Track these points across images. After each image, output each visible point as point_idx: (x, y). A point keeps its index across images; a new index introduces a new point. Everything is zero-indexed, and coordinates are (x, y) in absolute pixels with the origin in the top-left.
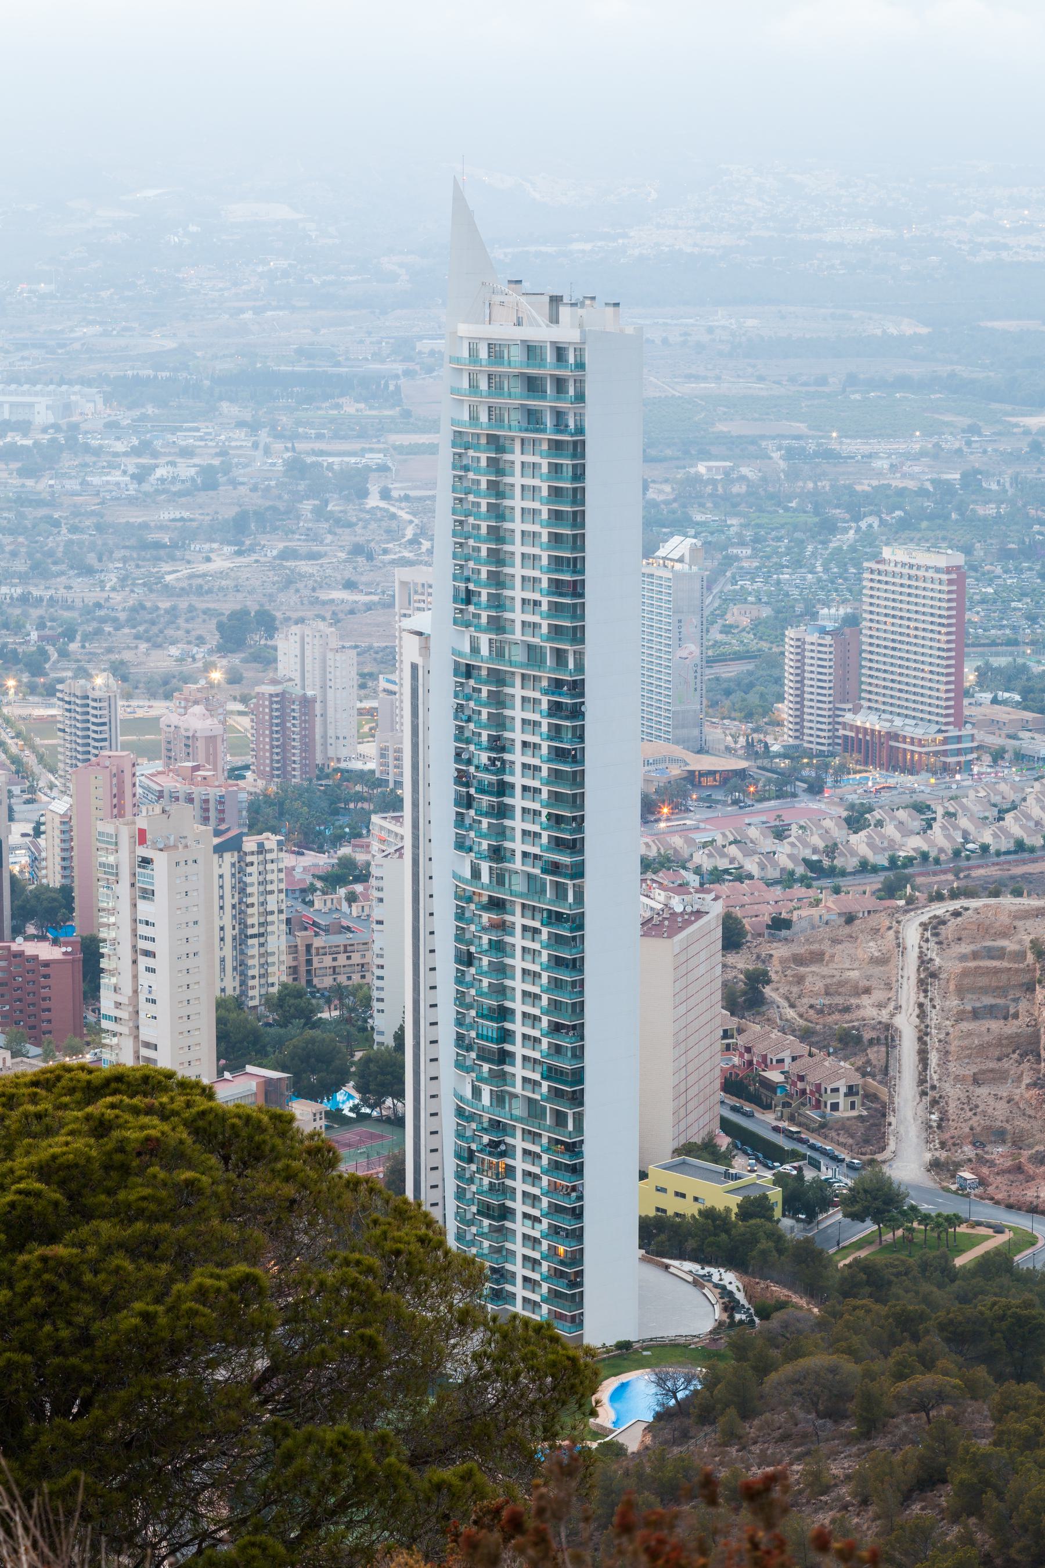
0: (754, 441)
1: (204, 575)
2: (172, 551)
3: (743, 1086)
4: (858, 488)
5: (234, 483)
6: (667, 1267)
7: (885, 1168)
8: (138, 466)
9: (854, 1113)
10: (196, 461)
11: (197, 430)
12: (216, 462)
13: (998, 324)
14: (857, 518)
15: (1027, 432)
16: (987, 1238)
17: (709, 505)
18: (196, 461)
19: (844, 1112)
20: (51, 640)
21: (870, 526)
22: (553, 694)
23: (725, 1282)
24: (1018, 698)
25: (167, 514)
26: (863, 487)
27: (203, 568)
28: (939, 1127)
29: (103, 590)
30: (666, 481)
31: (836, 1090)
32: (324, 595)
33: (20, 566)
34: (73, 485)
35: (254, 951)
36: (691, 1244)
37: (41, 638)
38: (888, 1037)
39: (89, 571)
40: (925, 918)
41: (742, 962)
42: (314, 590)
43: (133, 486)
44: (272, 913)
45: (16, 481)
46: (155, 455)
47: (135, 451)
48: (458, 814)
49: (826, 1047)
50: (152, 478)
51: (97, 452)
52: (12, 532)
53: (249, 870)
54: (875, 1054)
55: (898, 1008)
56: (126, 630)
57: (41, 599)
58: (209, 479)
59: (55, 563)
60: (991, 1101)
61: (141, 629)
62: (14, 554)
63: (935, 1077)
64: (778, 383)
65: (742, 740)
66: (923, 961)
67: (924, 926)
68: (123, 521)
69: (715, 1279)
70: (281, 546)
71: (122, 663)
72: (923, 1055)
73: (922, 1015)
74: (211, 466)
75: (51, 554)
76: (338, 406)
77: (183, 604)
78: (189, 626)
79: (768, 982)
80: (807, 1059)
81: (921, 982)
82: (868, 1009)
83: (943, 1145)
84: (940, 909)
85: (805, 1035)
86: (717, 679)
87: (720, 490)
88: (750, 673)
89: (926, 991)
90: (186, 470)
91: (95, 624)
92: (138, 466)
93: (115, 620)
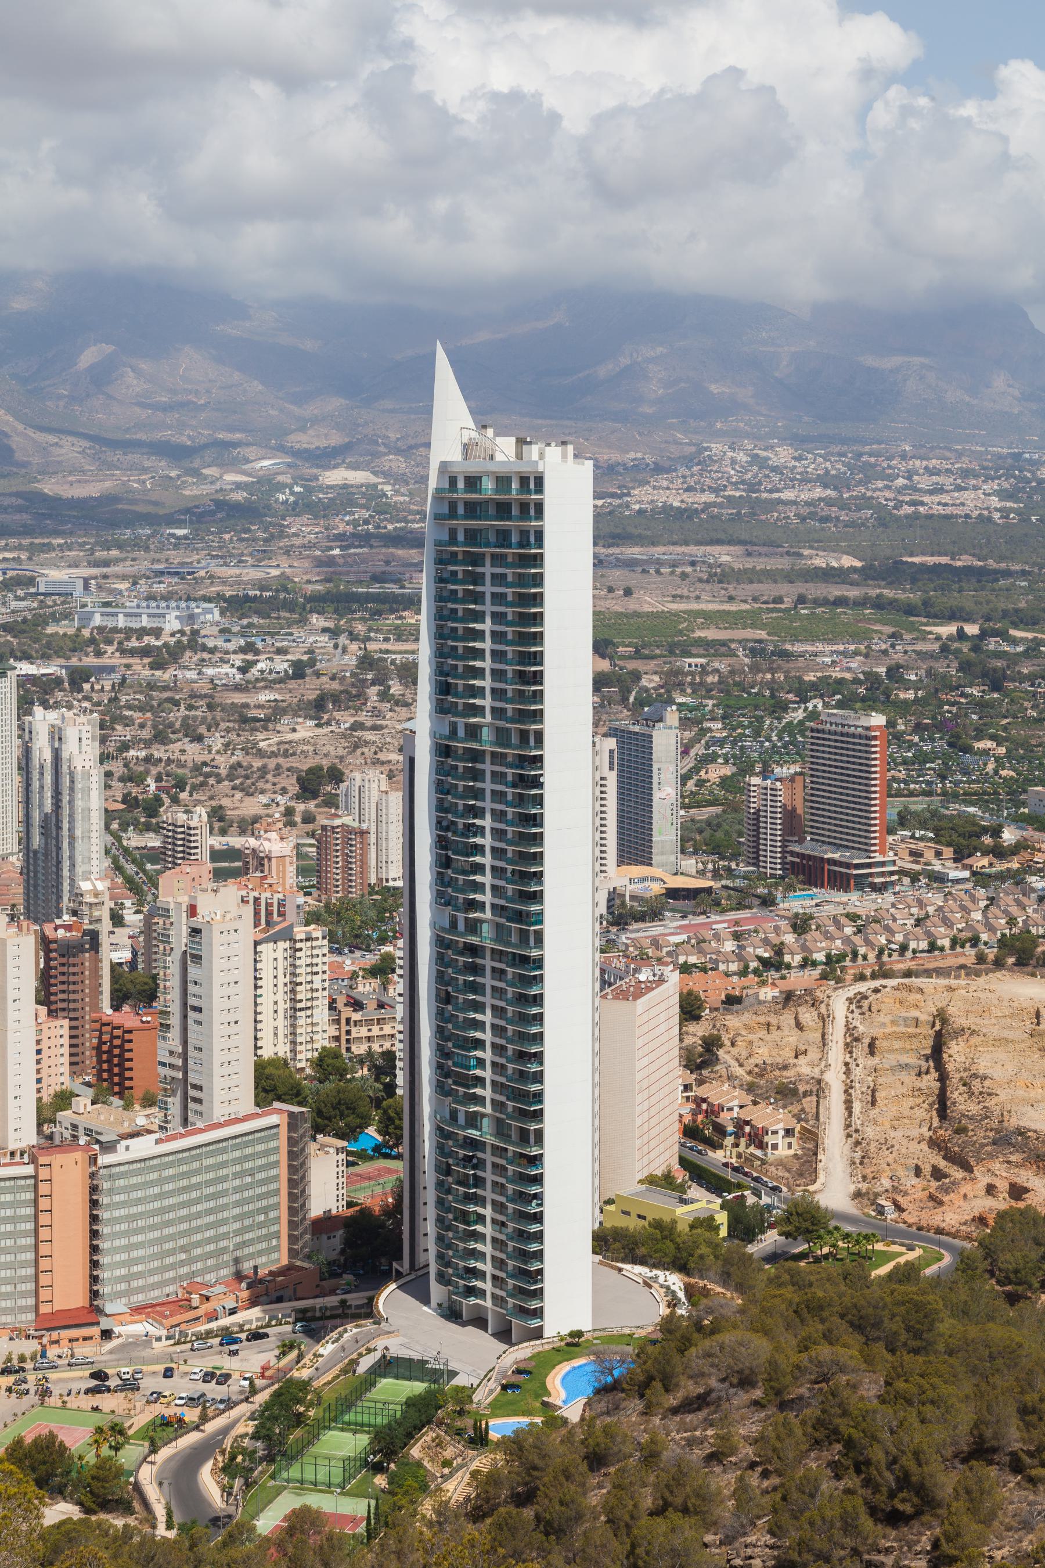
0: (724, 643)
1: (290, 742)
2: (266, 723)
3: (701, 1131)
4: (806, 678)
5: (318, 674)
6: (620, 1270)
7: (817, 1197)
8: (243, 661)
9: (792, 1152)
10: (289, 657)
11: (291, 634)
12: (305, 658)
13: (916, 560)
14: (804, 700)
15: (938, 638)
16: (901, 1254)
17: (689, 691)
18: (289, 657)
19: (783, 1152)
20: (166, 790)
21: (815, 706)
22: (517, 768)
23: (669, 1283)
24: (931, 835)
25: (264, 697)
26: (810, 677)
27: (290, 737)
28: (861, 1163)
29: (210, 752)
30: (656, 673)
31: (775, 1132)
32: (382, 756)
33: (146, 734)
34: (191, 675)
35: (301, 1022)
36: (642, 1251)
37: (158, 788)
38: (819, 1089)
39: (199, 739)
40: (851, 994)
41: (698, 1030)
42: (376, 753)
43: (239, 676)
44: (317, 990)
45: (147, 672)
46: (257, 652)
47: (242, 650)
48: (439, 873)
49: (768, 1098)
50: (254, 671)
51: (212, 651)
52: (141, 709)
53: (298, 954)
54: (809, 1103)
55: (828, 1066)
56: (226, 783)
57: (160, 760)
58: (299, 670)
59: (173, 733)
60: (905, 1142)
61: (238, 782)
62: (142, 726)
63: (859, 1122)
64: (745, 601)
65: (710, 866)
66: (849, 1029)
67: (850, 1000)
68: (229, 701)
69: (661, 1280)
70: (352, 720)
71: (221, 807)
72: (848, 1104)
73: (848, 1072)
74: (300, 661)
75: (171, 725)
76: (401, 618)
77: (272, 763)
78: (276, 780)
79: (721, 1046)
80: (751, 1107)
81: (847, 1045)
82: (804, 1067)
83: (864, 1178)
84: (863, 987)
85: (750, 1088)
86: (692, 820)
87: (698, 680)
88: (718, 816)
89: (851, 1052)
90: (281, 665)
91: (201, 779)
92: (243, 661)
93: (218, 775)
